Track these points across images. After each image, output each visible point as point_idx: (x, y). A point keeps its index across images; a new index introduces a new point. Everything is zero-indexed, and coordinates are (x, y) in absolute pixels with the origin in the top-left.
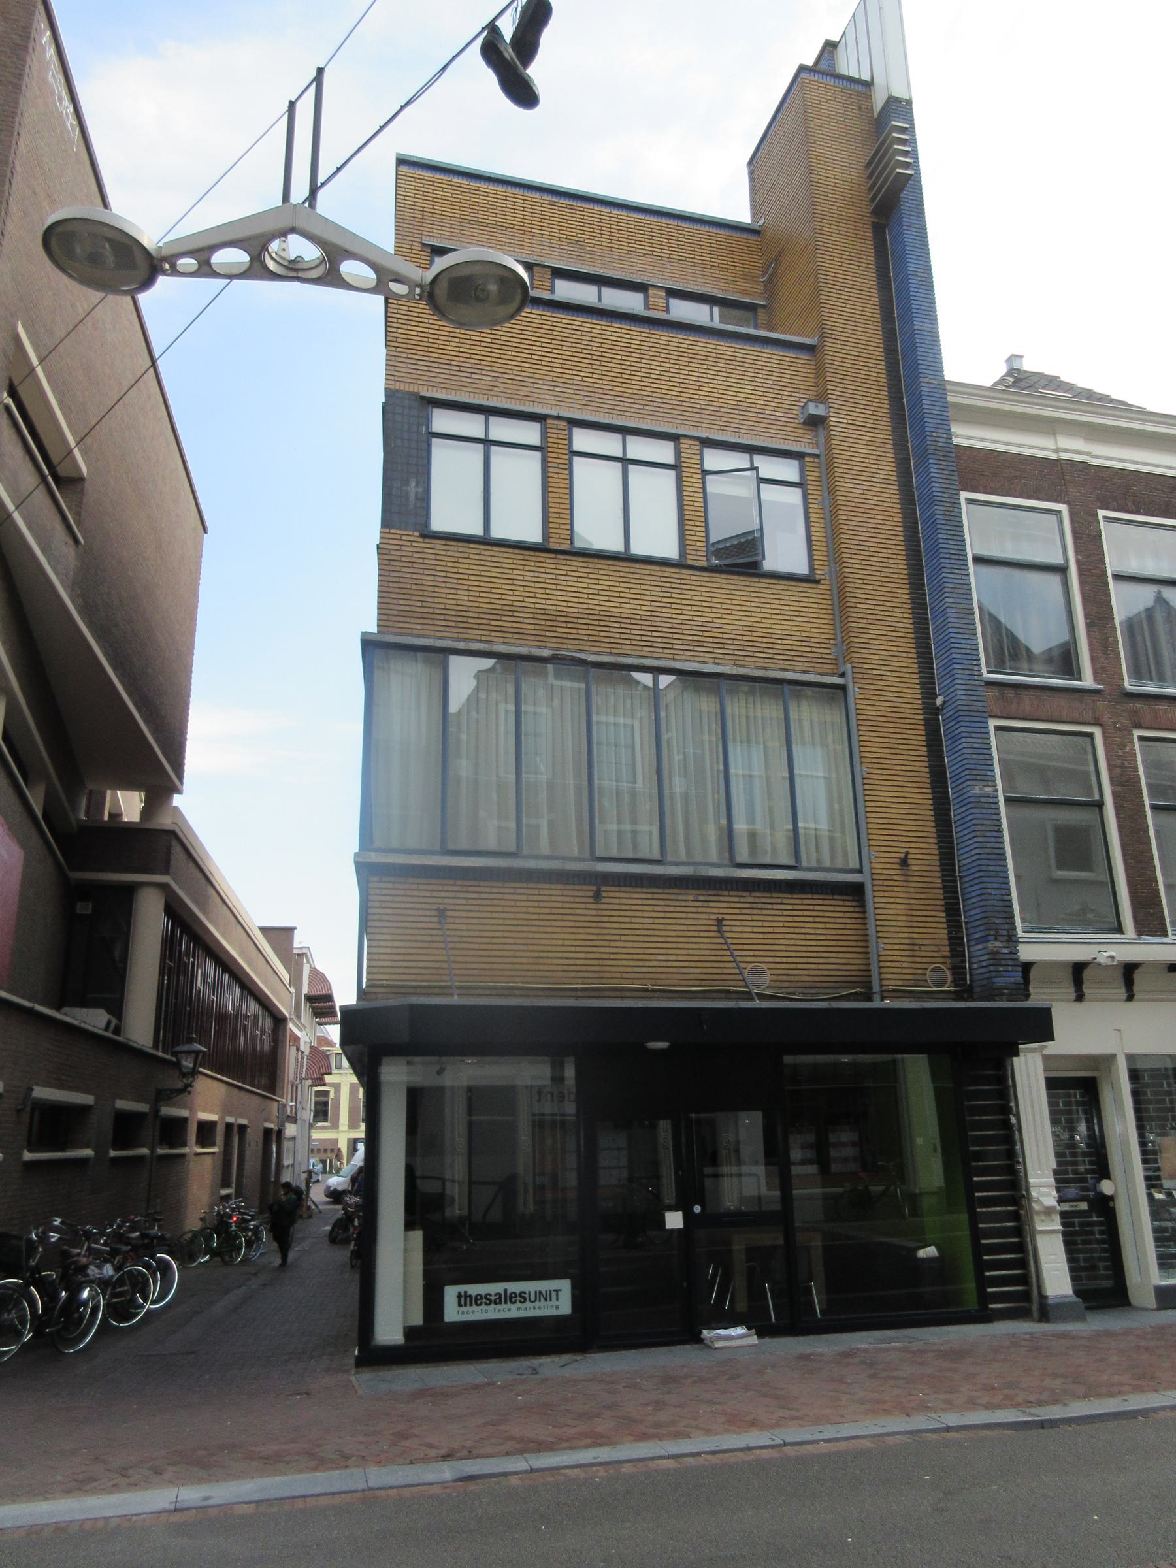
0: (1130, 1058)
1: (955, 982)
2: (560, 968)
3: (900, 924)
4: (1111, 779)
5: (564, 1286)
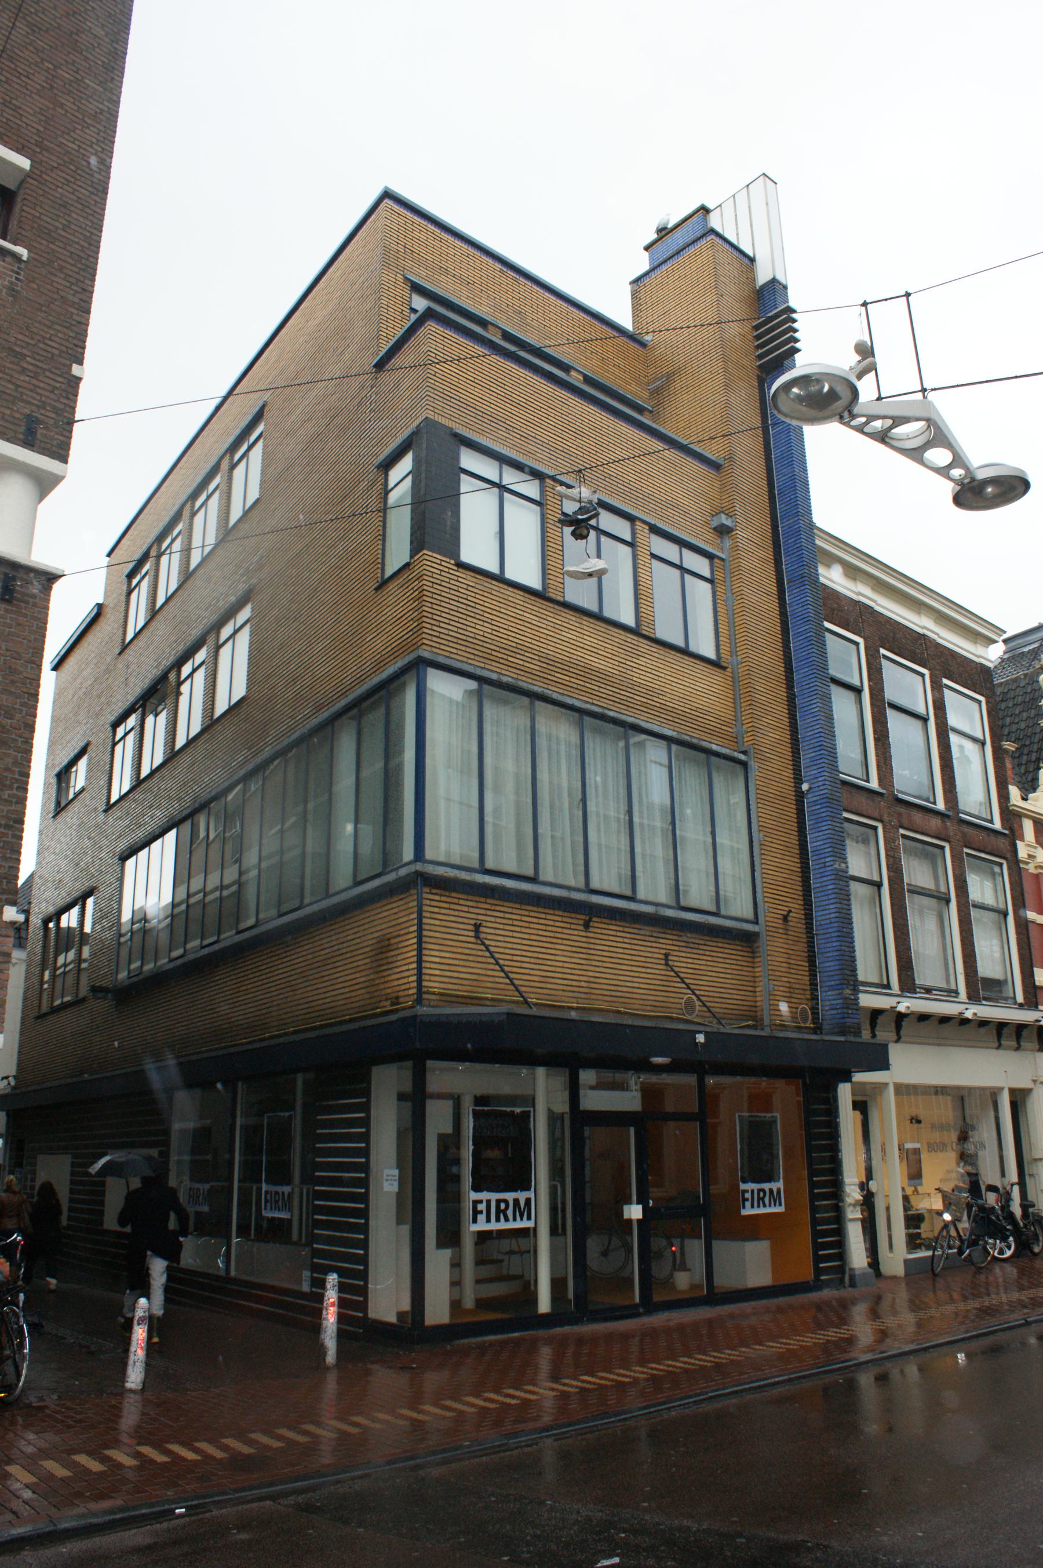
2: (561, 987)
4: (888, 865)
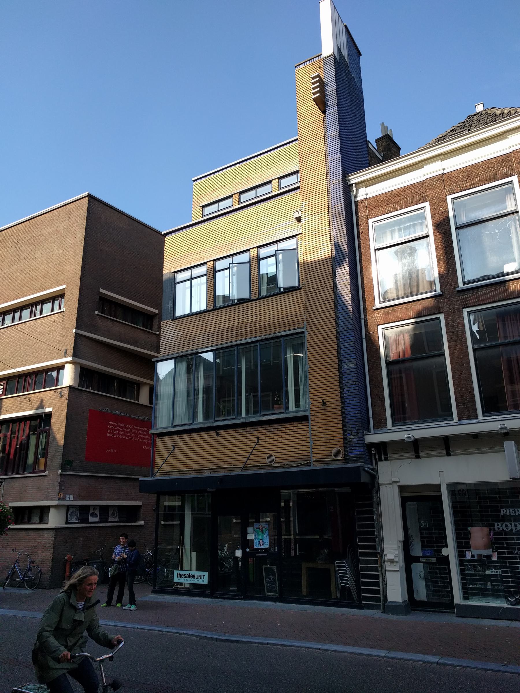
0: (448, 485)
1: (345, 455)
3: (321, 431)
5: (206, 574)
